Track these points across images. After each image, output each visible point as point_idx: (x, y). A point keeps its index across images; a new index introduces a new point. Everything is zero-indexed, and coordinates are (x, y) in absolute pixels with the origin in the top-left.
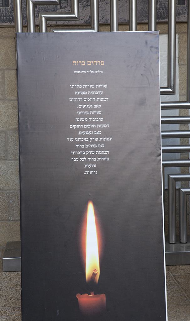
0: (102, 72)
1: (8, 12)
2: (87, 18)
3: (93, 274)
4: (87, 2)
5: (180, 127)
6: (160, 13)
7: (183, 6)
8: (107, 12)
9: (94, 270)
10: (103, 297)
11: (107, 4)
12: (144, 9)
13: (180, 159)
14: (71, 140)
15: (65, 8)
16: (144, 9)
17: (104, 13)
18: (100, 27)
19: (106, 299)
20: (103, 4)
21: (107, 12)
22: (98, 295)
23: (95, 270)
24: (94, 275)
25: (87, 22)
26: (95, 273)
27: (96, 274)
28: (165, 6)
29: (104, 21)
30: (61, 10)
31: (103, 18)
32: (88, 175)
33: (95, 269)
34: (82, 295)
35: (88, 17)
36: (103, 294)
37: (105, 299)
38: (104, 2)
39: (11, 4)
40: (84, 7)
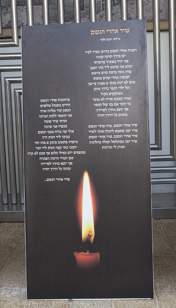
0: (119, 39)
2: (7, 22)
3: (88, 235)
4: (7, 10)
7: (83, 11)
8: (22, 17)
9: (90, 232)
10: (97, 255)
11: (22, 11)
12: (52, 14)
14: (60, 111)
16: (52, 14)
19: (100, 257)
21: (22, 17)
23: (90, 232)
24: (89, 236)
25: (7, 25)
26: (90, 234)
27: (91, 235)
28: (69, 11)
29: (20, 24)
34: (79, 253)
37: (99, 257)
38: (20, 10)
40: (5, 14)
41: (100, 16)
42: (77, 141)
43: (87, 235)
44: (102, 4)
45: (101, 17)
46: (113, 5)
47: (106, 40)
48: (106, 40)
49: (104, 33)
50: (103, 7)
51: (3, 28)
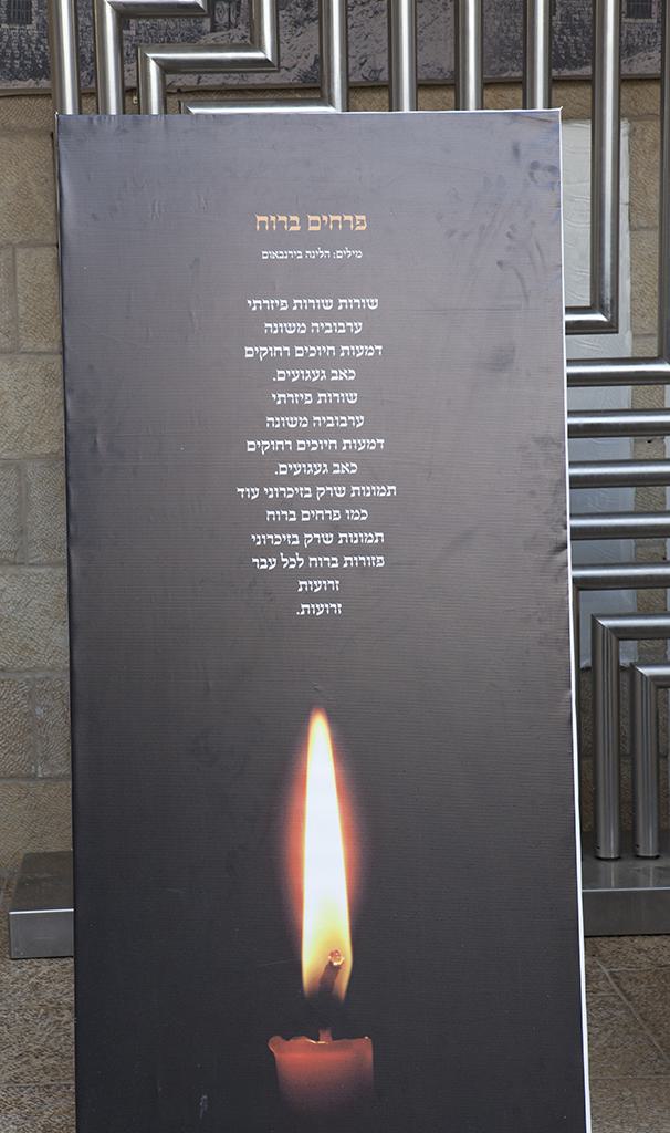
0: (359, 254)
1: (29, 41)
2: (306, 64)
3: (327, 968)
4: (306, 8)
5: (634, 449)
6: (566, 46)
7: (647, 20)
8: (377, 41)
9: (332, 954)
10: (362, 1050)
11: (376, 13)
12: (509, 30)
13: (633, 561)
14: (252, 494)
15: (229, 28)
16: (509, 30)
17: (365, 47)
18: (351, 94)
19: (374, 1056)
20: (362, 13)
21: (377, 41)
22: (345, 1040)
23: (335, 954)
24: (332, 970)
25: (305, 77)
26: (335, 964)
27: (338, 968)
28: (581, 20)
29: (366, 75)
30: (214, 35)
31: (362, 64)
32: (310, 617)
33: (334, 950)
34: (288, 1040)
35: (311, 61)
36: (363, 1037)
37: (370, 1055)
38: (367, 7)
39: (38, 13)
40: (297, 24)
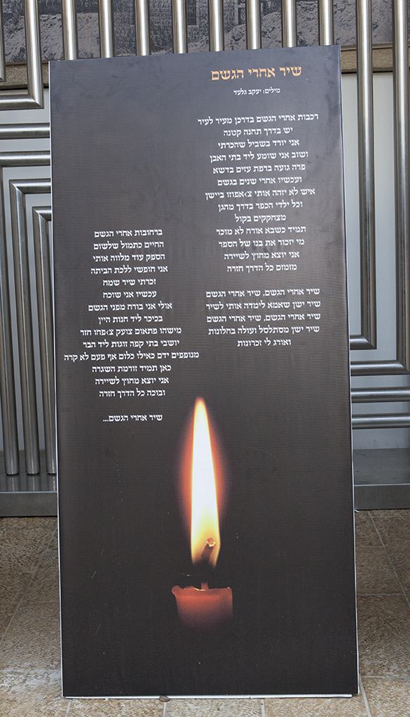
0: (278, 90)
2: (16, 52)
3: (206, 547)
4: (15, 24)
7: (194, 26)
8: (52, 39)
9: (209, 540)
10: (226, 594)
11: (51, 25)
12: (121, 32)
14: (140, 258)
16: (121, 32)
19: (233, 597)
21: (52, 39)
23: (210, 540)
24: (208, 549)
25: (15, 59)
26: (210, 546)
27: (212, 548)
28: (160, 27)
29: (47, 57)
32: (243, 348)
34: (183, 588)
37: (231, 597)
38: (47, 23)
40: (11, 32)
41: (233, 37)
42: (180, 329)
43: (204, 547)
44: (236, 10)
45: (236, 40)
46: (264, 11)
47: (248, 92)
48: (248, 92)
49: (243, 76)
50: (239, 16)
51: (7, 66)
